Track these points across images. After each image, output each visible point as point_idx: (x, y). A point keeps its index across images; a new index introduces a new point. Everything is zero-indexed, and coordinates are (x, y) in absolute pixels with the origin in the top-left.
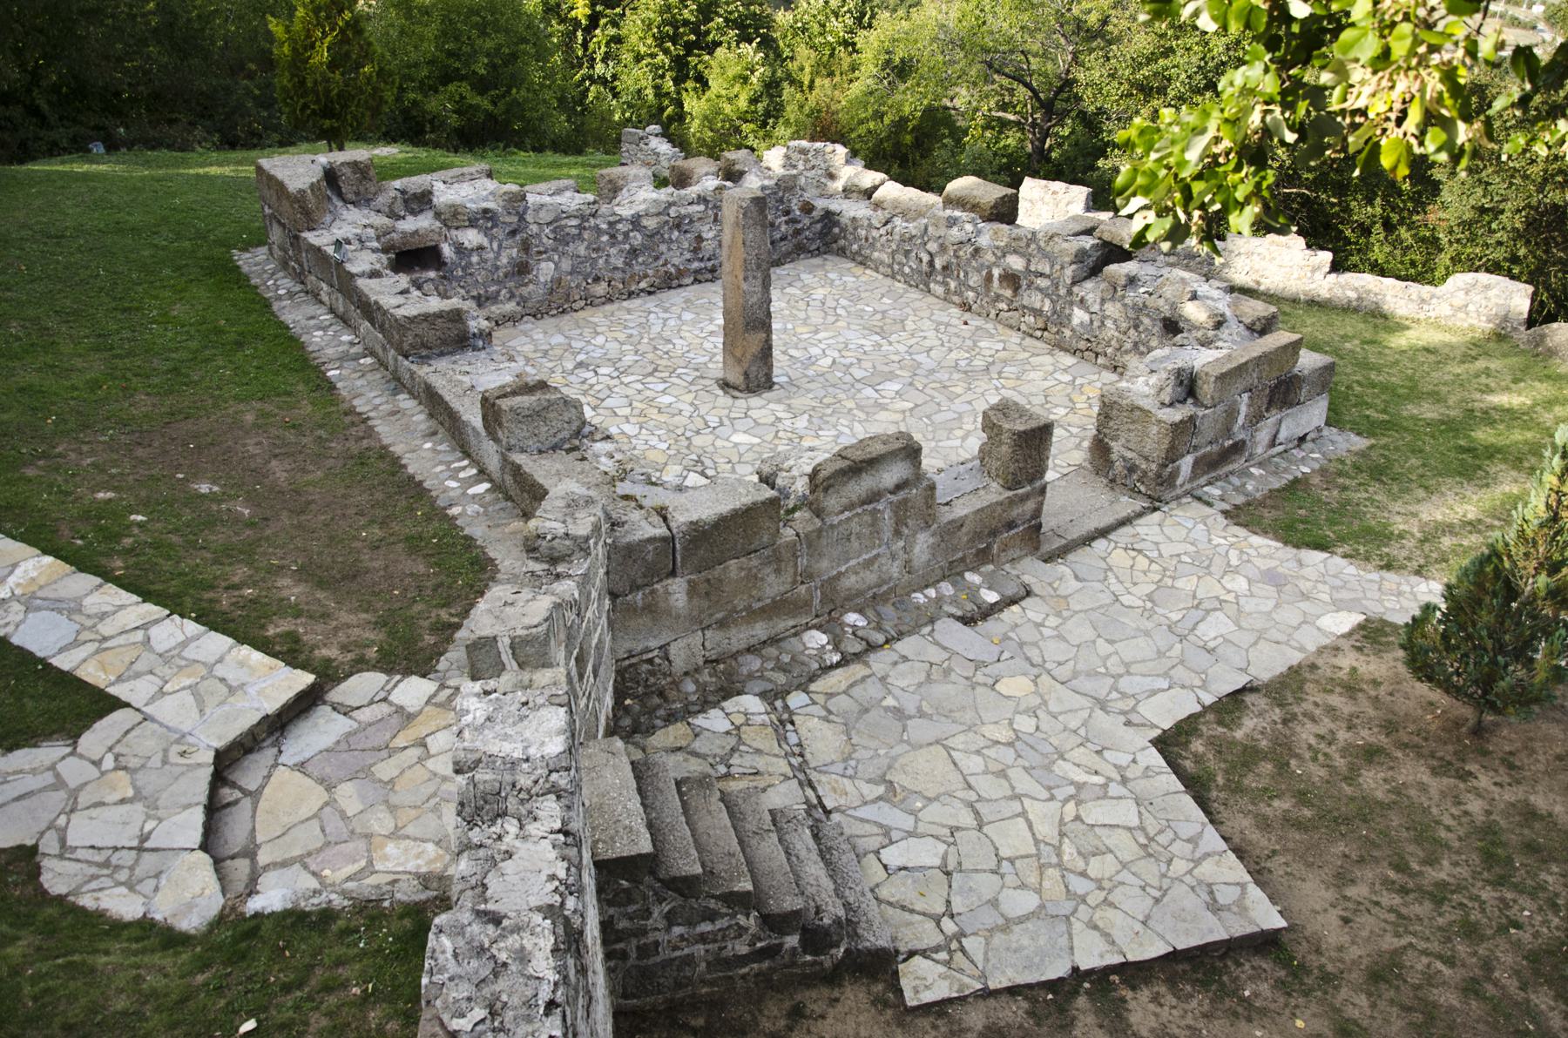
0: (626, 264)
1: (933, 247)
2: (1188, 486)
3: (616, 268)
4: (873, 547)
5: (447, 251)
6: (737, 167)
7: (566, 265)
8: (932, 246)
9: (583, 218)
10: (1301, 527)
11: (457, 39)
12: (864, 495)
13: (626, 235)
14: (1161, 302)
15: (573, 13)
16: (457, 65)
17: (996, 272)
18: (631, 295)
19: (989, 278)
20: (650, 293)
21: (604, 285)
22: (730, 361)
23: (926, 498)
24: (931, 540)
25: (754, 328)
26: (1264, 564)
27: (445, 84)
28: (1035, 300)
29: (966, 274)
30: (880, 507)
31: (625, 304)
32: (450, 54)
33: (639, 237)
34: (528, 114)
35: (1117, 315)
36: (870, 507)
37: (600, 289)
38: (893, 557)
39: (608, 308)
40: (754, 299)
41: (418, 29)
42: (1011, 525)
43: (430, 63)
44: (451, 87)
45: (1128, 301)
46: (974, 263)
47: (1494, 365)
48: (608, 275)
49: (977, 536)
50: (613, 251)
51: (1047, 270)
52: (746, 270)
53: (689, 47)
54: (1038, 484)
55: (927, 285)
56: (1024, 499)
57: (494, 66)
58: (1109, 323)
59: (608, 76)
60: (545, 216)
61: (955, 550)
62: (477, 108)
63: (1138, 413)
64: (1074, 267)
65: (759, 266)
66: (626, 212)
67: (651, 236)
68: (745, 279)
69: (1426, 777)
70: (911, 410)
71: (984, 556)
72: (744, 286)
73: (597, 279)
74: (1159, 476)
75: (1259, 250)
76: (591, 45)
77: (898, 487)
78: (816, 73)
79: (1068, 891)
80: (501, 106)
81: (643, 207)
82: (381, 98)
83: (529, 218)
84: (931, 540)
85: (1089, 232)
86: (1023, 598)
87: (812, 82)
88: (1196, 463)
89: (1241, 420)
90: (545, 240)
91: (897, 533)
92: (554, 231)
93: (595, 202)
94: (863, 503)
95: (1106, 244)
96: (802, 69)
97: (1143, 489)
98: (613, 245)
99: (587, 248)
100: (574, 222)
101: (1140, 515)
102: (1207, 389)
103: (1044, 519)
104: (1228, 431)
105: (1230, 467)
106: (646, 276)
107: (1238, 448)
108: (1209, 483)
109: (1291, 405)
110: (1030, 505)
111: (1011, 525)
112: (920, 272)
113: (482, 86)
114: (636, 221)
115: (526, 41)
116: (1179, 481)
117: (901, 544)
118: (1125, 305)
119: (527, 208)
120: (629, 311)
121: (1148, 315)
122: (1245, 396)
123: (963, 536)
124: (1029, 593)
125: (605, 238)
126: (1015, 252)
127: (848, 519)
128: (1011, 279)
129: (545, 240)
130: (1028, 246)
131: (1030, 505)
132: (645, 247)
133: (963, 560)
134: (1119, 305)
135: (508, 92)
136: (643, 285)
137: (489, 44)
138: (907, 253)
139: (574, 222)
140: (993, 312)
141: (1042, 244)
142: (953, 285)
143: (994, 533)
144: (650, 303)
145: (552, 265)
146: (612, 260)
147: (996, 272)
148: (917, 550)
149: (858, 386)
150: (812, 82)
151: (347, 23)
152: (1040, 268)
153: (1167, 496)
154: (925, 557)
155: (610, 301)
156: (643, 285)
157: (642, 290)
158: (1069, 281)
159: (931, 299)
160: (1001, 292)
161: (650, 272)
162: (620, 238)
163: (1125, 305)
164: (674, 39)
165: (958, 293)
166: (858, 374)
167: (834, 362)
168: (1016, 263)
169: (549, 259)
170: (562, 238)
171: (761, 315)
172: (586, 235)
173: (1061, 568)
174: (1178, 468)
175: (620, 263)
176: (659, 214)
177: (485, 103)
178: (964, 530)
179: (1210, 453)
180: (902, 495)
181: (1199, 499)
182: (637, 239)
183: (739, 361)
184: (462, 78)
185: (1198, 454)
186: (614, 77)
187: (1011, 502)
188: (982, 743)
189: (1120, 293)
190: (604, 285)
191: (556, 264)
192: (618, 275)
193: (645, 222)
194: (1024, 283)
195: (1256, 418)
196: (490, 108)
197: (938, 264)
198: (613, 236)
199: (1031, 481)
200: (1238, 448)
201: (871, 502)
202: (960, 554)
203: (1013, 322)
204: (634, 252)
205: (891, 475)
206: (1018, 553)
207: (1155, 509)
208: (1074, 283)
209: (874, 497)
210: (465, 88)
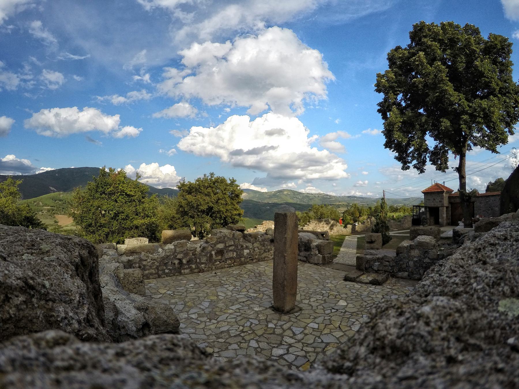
5: (202, 240)
8: (180, 256)
14: (269, 236)
17: (213, 253)
19: (211, 255)
28: (231, 255)
29: (200, 259)
35: (258, 245)
47: (390, 214)
51: (233, 243)
58: (256, 249)
69: (182, 200)
79: (177, 84)
112: (175, 269)
128: (220, 252)
130: (224, 238)
138: (166, 264)
142: (194, 266)
147: (213, 253)
152: (230, 244)
163: (260, 242)
165: (197, 268)
168: (220, 246)
188: (242, 315)
197: (184, 261)
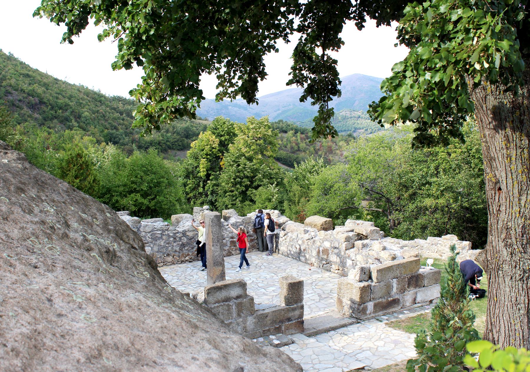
0: (180, 249)
1: (300, 242)
2: (372, 315)
3: (176, 251)
4: (229, 319)
6: (227, 215)
7: (156, 249)
9: (163, 231)
10: (416, 327)
11: (136, 177)
12: (223, 298)
13: (180, 238)
14: (374, 252)
15: (199, 174)
16: (135, 186)
18: (182, 262)
20: (190, 262)
21: (171, 257)
22: (209, 278)
23: (250, 303)
24: (254, 320)
25: (217, 265)
26: (393, 338)
27: (130, 194)
30: (231, 304)
31: (179, 265)
32: (133, 182)
33: (185, 239)
34: (163, 206)
36: (227, 303)
37: (170, 259)
38: (238, 324)
39: (173, 266)
40: (217, 254)
41: (121, 172)
42: (289, 319)
43: (125, 185)
44: (132, 195)
45: (363, 254)
46: (314, 247)
48: (173, 254)
49: (274, 322)
50: (175, 244)
52: (213, 242)
53: (247, 187)
54: (299, 304)
55: (299, 258)
56: (294, 310)
57: (151, 188)
59: (213, 200)
60: (148, 229)
61: (265, 326)
62: (142, 203)
63: (349, 285)
64: (346, 243)
65: (218, 241)
66: (180, 230)
67: (190, 239)
68: (213, 246)
70: (276, 295)
71: (278, 330)
72: (213, 248)
73: (168, 255)
74: (358, 309)
75: (440, 242)
76: (206, 187)
77: (238, 297)
78: (300, 197)
80: (153, 203)
81: (187, 228)
82: (94, 189)
83: (141, 229)
84: (254, 320)
85: (352, 231)
86: (290, 344)
87: (299, 200)
88: (375, 306)
89: (395, 290)
90: (148, 238)
91: (239, 315)
92: (151, 235)
93: (167, 225)
94: (223, 301)
95: (358, 234)
96: (295, 195)
97: (354, 315)
98: (175, 242)
99: (164, 243)
100: (160, 232)
101: (351, 324)
102: (374, 275)
103: (305, 317)
104: (389, 294)
105: (394, 310)
106: (188, 255)
107: (395, 302)
108: (384, 315)
109: (420, 287)
110: (297, 313)
111: (289, 319)
113: (145, 195)
114: (184, 233)
115: (163, 177)
116: (368, 312)
117: (241, 320)
118: (362, 255)
119: (141, 226)
120: (180, 267)
121: (370, 258)
122: (395, 280)
123: (268, 320)
124: (293, 343)
125: (172, 239)
126: (327, 240)
127: (218, 306)
129: (148, 238)
131: (297, 313)
132: (188, 244)
133: (269, 330)
134: (360, 256)
135: (155, 197)
136: (187, 258)
137: (149, 178)
139: (160, 232)
140: (321, 265)
141: (335, 236)
143: (282, 322)
144: (189, 265)
145: (150, 248)
146: (175, 248)
148: (248, 323)
149: (259, 288)
150: (299, 200)
151: (83, 162)
153: (363, 317)
154: (252, 327)
155: (173, 264)
156: (187, 258)
157: (187, 261)
158: (344, 249)
159: (300, 263)
160: (323, 257)
161: (190, 253)
162: (178, 239)
164: (240, 183)
166: (260, 285)
167: (253, 282)
169: (149, 246)
170: (155, 239)
171: (220, 260)
172: (164, 237)
173: (312, 340)
174: (366, 307)
175: (178, 249)
176: (194, 231)
177: (146, 202)
178: (268, 318)
179: (382, 302)
180: (239, 300)
181: (378, 320)
182: (185, 240)
183: (212, 278)
184: (138, 192)
185: (376, 302)
186: (216, 200)
187: (288, 310)
189: (361, 251)
190: (171, 257)
191: (152, 248)
192: (177, 254)
193: (188, 234)
194: (330, 252)
195: (402, 291)
196: (148, 203)
198: (175, 238)
199: (296, 302)
200: (395, 302)
201: (226, 301)
202: (267, 328)
203: (328, 268)
204: (183, 245)
205: (235, 292)
206: (294, 332)
207: (358, 323)
208: (346, 250)
209: (228, 299)
210: (138, 196)
